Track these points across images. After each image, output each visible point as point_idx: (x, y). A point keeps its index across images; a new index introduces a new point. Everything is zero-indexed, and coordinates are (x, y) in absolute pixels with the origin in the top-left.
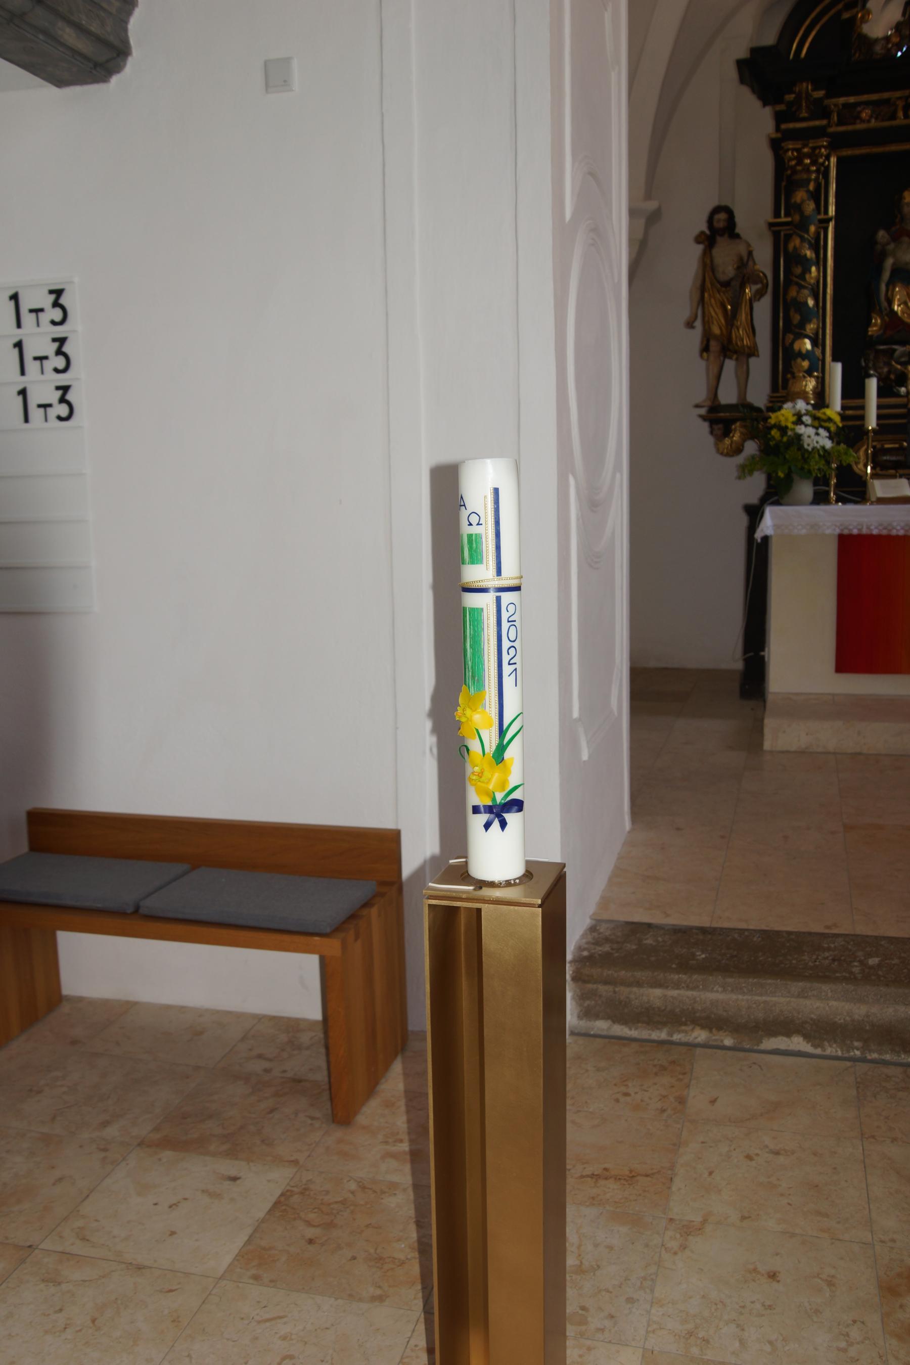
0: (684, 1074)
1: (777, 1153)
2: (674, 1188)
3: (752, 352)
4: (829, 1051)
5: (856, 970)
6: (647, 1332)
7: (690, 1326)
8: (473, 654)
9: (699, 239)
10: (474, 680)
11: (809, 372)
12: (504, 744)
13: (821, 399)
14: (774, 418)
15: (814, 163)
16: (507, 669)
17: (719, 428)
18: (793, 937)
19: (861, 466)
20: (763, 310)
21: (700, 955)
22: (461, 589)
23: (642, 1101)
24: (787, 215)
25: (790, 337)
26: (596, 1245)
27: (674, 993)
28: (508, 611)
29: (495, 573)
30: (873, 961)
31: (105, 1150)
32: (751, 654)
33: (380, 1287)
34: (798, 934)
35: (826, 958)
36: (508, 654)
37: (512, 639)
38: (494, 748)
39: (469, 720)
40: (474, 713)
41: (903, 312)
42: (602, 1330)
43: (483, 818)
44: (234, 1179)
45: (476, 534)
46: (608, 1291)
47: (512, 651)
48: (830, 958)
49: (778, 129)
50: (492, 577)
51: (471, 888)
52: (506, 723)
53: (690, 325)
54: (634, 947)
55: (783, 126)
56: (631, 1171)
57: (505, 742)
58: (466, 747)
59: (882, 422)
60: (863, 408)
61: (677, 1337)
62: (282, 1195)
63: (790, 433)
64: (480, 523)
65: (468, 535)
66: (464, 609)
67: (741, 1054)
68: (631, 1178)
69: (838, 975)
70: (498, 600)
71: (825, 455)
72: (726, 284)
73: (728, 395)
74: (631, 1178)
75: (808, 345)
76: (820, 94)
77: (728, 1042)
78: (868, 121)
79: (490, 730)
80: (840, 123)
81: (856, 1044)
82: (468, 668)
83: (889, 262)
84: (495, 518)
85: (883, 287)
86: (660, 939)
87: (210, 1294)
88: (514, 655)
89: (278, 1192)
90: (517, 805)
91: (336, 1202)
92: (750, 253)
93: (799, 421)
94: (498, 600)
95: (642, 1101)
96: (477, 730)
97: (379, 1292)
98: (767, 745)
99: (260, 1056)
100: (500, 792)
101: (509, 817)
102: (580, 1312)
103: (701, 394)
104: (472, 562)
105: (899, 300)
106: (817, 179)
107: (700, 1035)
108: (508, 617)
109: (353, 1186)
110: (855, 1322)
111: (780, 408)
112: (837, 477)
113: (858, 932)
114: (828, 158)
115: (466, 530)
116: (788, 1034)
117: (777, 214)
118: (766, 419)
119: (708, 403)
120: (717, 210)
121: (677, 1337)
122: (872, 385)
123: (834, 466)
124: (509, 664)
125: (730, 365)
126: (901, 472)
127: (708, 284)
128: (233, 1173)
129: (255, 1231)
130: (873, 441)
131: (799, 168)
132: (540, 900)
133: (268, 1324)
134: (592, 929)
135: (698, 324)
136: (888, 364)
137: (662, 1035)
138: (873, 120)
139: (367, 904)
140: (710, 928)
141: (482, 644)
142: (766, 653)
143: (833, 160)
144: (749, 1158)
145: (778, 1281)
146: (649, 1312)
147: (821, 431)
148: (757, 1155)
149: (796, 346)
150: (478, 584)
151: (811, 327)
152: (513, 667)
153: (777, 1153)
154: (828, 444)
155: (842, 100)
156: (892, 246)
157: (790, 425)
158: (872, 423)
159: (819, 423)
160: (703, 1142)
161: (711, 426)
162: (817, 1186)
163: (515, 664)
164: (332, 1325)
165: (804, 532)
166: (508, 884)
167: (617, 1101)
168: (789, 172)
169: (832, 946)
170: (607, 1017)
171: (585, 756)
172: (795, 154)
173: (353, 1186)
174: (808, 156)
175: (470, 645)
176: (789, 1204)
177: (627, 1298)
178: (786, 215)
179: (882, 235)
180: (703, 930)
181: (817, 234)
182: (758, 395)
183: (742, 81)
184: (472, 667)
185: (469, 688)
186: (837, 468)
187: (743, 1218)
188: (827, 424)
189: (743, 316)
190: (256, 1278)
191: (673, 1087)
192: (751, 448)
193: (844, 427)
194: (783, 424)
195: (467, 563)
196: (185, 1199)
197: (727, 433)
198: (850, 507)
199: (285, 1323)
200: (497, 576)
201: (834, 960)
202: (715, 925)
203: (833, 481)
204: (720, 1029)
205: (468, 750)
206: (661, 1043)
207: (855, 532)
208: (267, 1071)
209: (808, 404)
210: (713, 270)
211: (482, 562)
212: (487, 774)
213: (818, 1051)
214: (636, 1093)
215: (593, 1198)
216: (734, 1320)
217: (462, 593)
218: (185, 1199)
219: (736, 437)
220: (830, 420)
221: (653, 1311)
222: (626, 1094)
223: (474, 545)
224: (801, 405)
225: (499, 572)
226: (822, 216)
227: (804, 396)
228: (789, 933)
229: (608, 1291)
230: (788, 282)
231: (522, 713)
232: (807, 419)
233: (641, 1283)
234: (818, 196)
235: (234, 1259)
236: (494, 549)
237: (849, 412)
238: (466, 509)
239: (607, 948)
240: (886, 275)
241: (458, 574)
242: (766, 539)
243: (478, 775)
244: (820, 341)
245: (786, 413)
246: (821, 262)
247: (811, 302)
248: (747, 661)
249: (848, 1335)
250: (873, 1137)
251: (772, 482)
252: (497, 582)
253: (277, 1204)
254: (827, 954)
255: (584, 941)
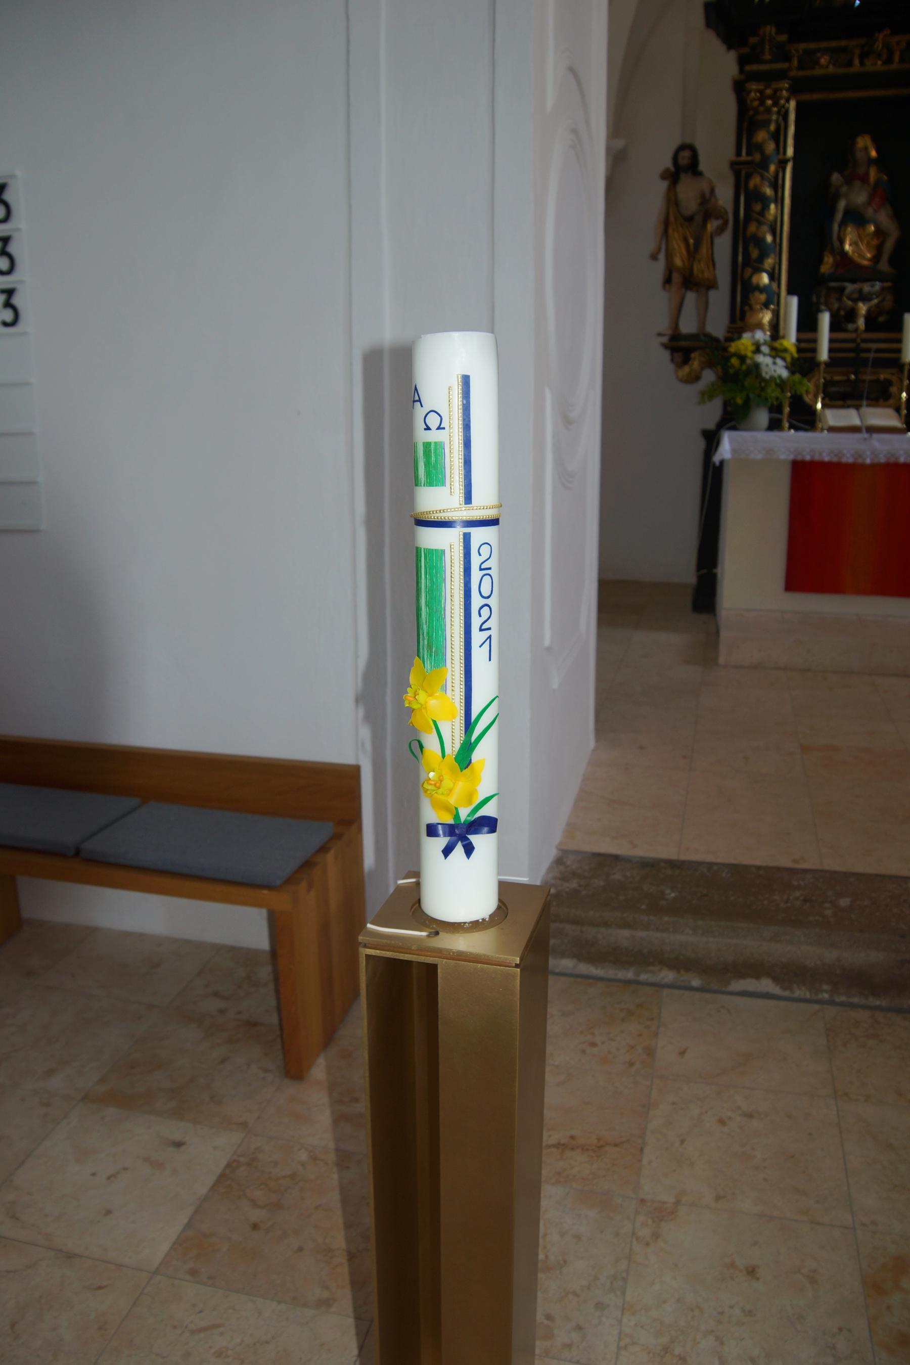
0: (652, 1019)
1: (750, 1116)
2: (645, 1161)
3: (712, 285)
4: (798, 993)
5: (828, 912)
6: (619, 1348)
7: (665, 1340)
8: (430, 615)
9: (665, 175)
10: (431, 652)
11: (766, 305)
12: (472, 742)
13: (776, 331)
14: (733, 347)
15: (775, 104)
16: (477, 637)
17: (679, 356)
18: (762, 872)
19: (811, 396)
20: (723, 245)
21: (670, 894)
22: (413, 521)
23: (609, 1052)
24: (749, 153)
25: (749, 271)
26: (563, 1234)
27: (644, 934)
28: (480, 555)
29: (462, 499)
30: (844, 902)
31: (47, 1105)
32: (705, 571)
33: (327, 1288)
34: (767, 869)
35: (797, 899)
36: (480, 615)
37: (485, 594)
38: (457, 746)
39: (424, 707)
40: (430, 698)
41: (854, 252)
42: (569, 1346)
43: (442, 842)
44: (179, 1144)
45: (436, 443)
46: (575, 1294)
47: (485, 612)
48: (801, 898)
49: (741, 71)
50: (458, 506)
51: (424, 934)
52: (474, 714)
53: (654, 257)
54: (602, 883)
55: (748, 68)
56: (599, 1140)
57: (473, 738)
58: (419, 742)
59: (834, 355)
60: (815, 341)
61: (651, 1355)
62: (228, 1165)
63: (748, 361)
64: (441, 426)
65: (424, 443)
66: (418, 550)
67: (708, 996)
68: (599, 1148)
69: (811, 918)
70: (467, 538)
71: (781, 384)
72: (689, 219)
73: (688, 326)
74: (599, 1148)
75: (765, 279)
76: (783, 38)
77: (696, 983)
78: (825, 65)
79: (453, 722)
80: (800, 67)
81: (825, 987)
82: (423, 634)
83: (842, 205)
84: (464, 420)
85: (836, 227)
86: (628, 874)
87: (141, 1294)
88: (488, 557)
89: (223, 1163)
90: (489, 824)
91: (285, 1177)
92: (712, 191)
93: (757, 350)
94: (467, 538)
95: (609, 1052)
96: (435, 722)
97: (325, 1294)
98: (722, 660)
99: (216, 994)
100: (465, 807)
101: (475, 839)
102: (546, 1322)
103: (663, 324)
104: (430, 484)
105: (851, 240)
106: (777, 121)
107: (668, 976)
108: (479, 564)
109: (303, 1156)
110: (840, 1329)
111: (740, 338)
112: (791, 406)
113: (826, 868)
114: (788, 101)
115: (422, 437)
116: (757, 977)
117: (738, 153)
118: (725, 349)
119: (669, 332)
120: (682, 148)
121: (651, 1355)
122: (825, 319)
123: (789, 394)
124: (481, 630)
125: (691, 297)
126: (849, 402)
127: (672, 219)
128: (177, 1137)
129: (196, 1212)
130: (825, 372)
131: (761, 109)
132: (519, 958)
133: (202, 1335)
134: (559, 861)
135: (662, 256)
136: (839, 300)
137: (629, 975)
138: (831, 67)
139: (323, 849)
140: (678, 861)
141: (443, 601)
142: (719, 571)
143: (792, 104)
144: (722, 1122)
145: (758, 1279)
146: (620, 1321)
147: (779, 361)
148: (730, 1118)
149: (755, 280)
150: (434, 515)
151: (769, 262)
152: (486, 634)
153: (750, 1116)
154: (785, 374)
155: (802, 46)
156: (844, 189)
157: (749, 354)
158: (824, 354)
159: (777, 352)
160: (673, 1103)
161: (672, 354)
162: (793, 1156)
163: (489, 629)
164: (273, 1338)
165: (759, 457)
166: (476, 926)
167: (583, 1052)
168: (751, 113)
169: (802, 883)
170: (574, 956)
171: (555, 686)
172: (758, 94)
173: (303, 1156)
174: (769, 97)
175: (426, 602)
176: (765, 1180)
177: (597, 1304)
178: (748, 154)
179: (836, 178)
180: (672, 864)
181: (776, 177)
182: (717, 326)
183: (709, 24)
184: (428, 633)
185: (424, 663)
186: (792, 397)
187: (718, 1198)
188: (783, 355)
189: (704, 251)
190: (193, 1272)
191: (640, 1035)
192: (709, 376)
193: (798, 359)
194: (743, 353)
195: (422, 485)
196: (126, 1169)
197: (686, 361)
198: (801, 434)
199: (221, 1334)
200: (465, 504)
201: (805, 901)
202: (683, 857)
203: (787, 410)
204: (688, 970)
205: (421, 747)
206: (628, 982)
207: (808, 458)
208: (222, 1012)
209: (765, 334)
210: (677, 204)
211: (444, 484)
212: (447, 783)
213: (787, 993)
214: (603, 1043)
215: (559, 1174)
216: (713, 1331)
217: (415, 526)
218: (126, 1169)
219: (696, 364)
220: (785, 350)
221: (625, 1320)
222: (593, 1044)
223: (433, 459)
224: (760, 336)
225: (468, 499)
226: (781, 157)
227: (760, 326)
228: (759, 868)
229: (575, 1294)
230: (748, 218)
231: (497, 697)
232: (765, 349)
233: (612, 1283)
234: (778, 137)
235: (171, 1248)
236: (462, 465)
237: (803, 345)
238: (422, 406)
239: (574, 884)
240: (839, 216)
241: (411, 499)
242: (722, 462)
243: (435, 785)
244: (776, 276)
245: (745, 342)
246: (779, 201)
247: (769, 238)
248: (700, 578)
249: (834, 1348)
250: (846, 1094)
251: (729, 409)
252: (465, 513)
253: (222, 1177)
254: (797, 894)
255: (551, 875)
